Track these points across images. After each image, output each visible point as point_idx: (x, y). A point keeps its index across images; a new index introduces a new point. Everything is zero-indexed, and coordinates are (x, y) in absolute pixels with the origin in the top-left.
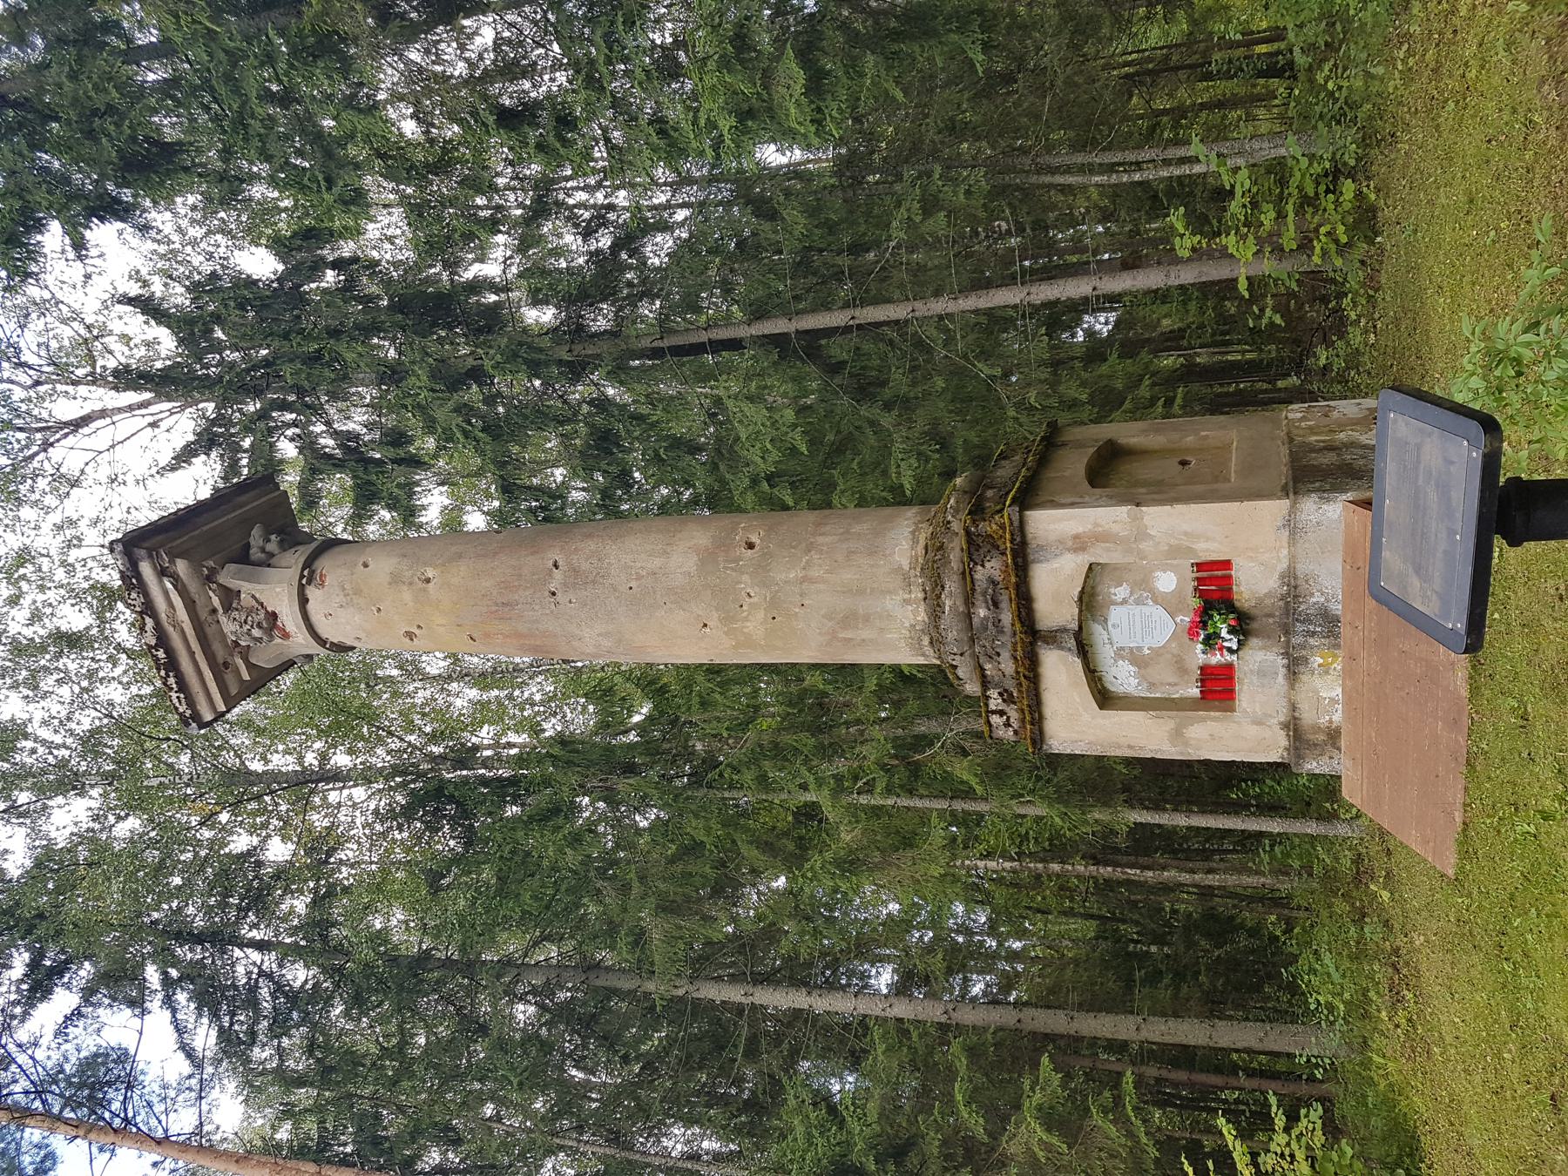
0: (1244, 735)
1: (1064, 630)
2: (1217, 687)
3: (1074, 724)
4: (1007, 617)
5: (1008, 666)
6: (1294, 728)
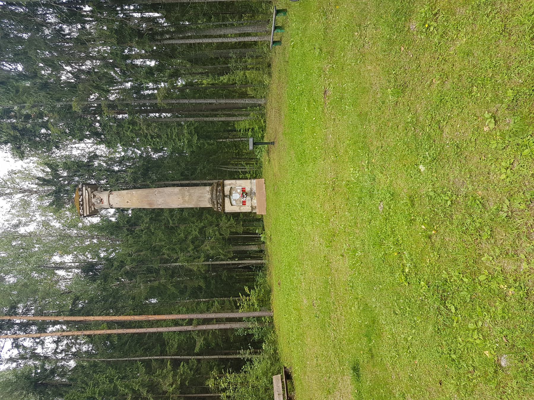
0: (246, 209)
2: (244, 203)
3: (229, 208)
5: (221, 201)
6: (252, 207)
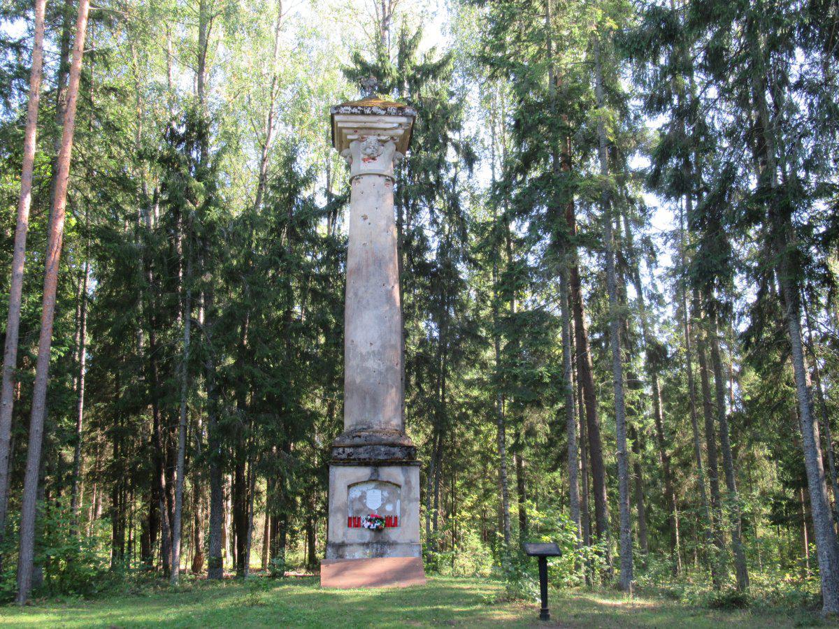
1: (378, 476)
2: (354, 522)
4: (381, 457)
